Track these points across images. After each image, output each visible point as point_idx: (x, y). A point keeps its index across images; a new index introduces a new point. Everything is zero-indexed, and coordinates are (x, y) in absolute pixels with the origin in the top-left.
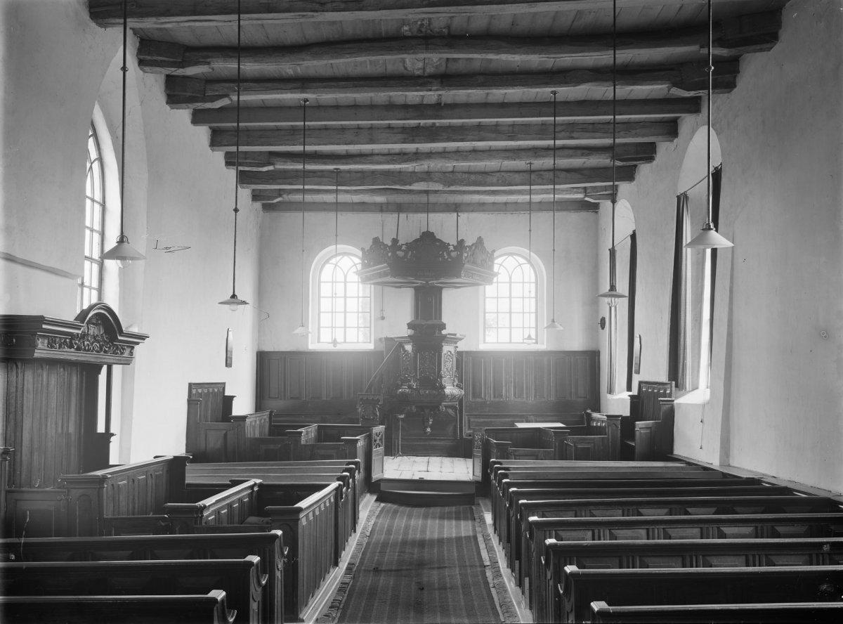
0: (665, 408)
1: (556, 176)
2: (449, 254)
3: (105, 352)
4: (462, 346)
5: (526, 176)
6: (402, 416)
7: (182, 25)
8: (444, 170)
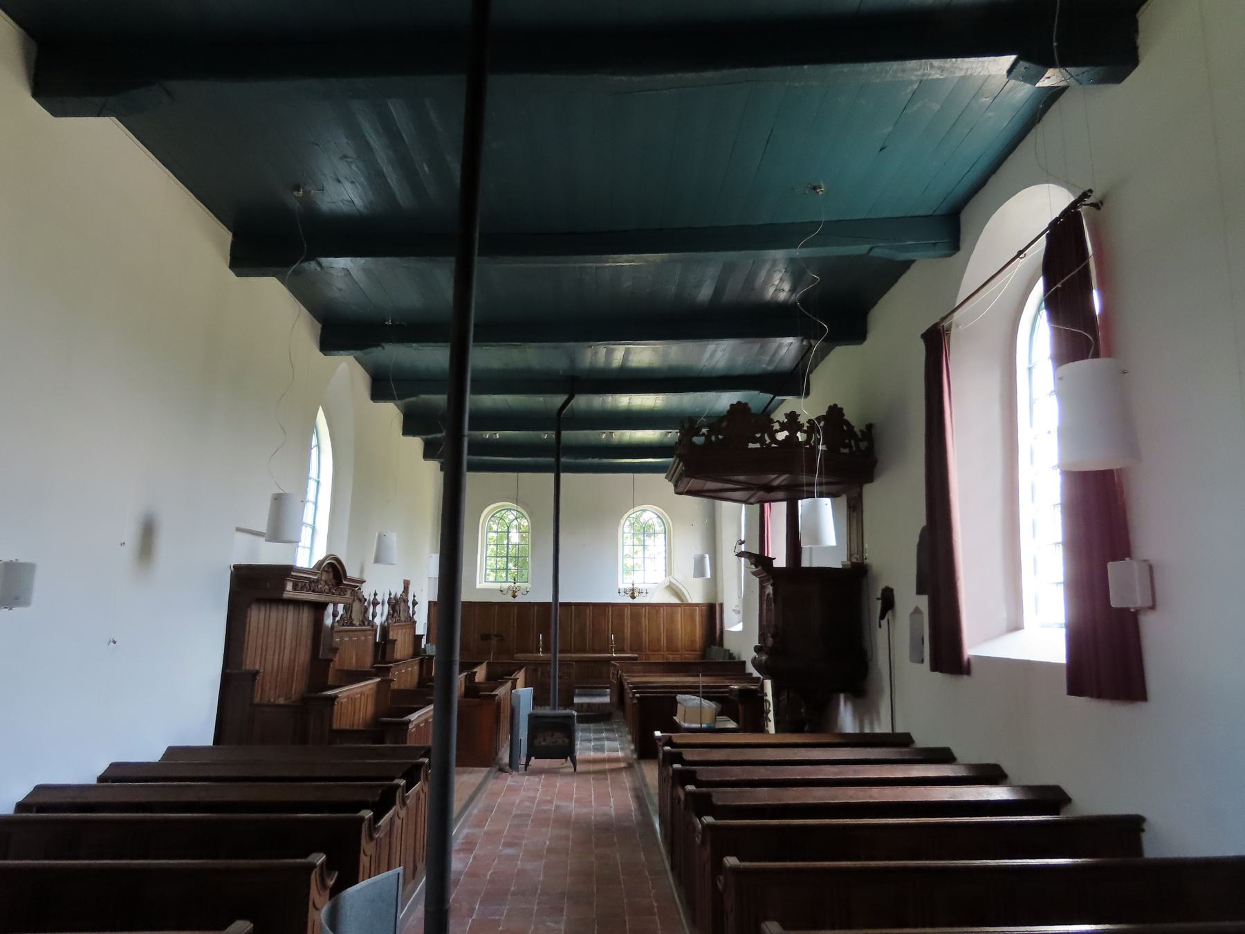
3: (333, 593)
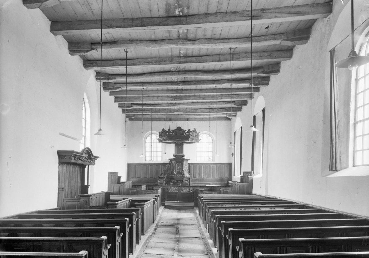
0: (250, 179)
1: (217, 110)
2: (185, 134)
4: (190, 162)
5: (209, 110)
6: (172, 183)
7: (109, 69)
8: (184, 108)
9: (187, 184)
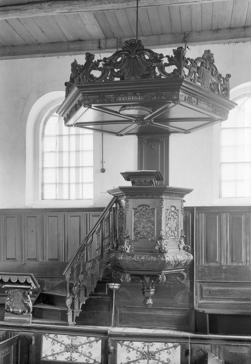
2: (162, 69)
4: (190, 201)
9: (183, 287)
